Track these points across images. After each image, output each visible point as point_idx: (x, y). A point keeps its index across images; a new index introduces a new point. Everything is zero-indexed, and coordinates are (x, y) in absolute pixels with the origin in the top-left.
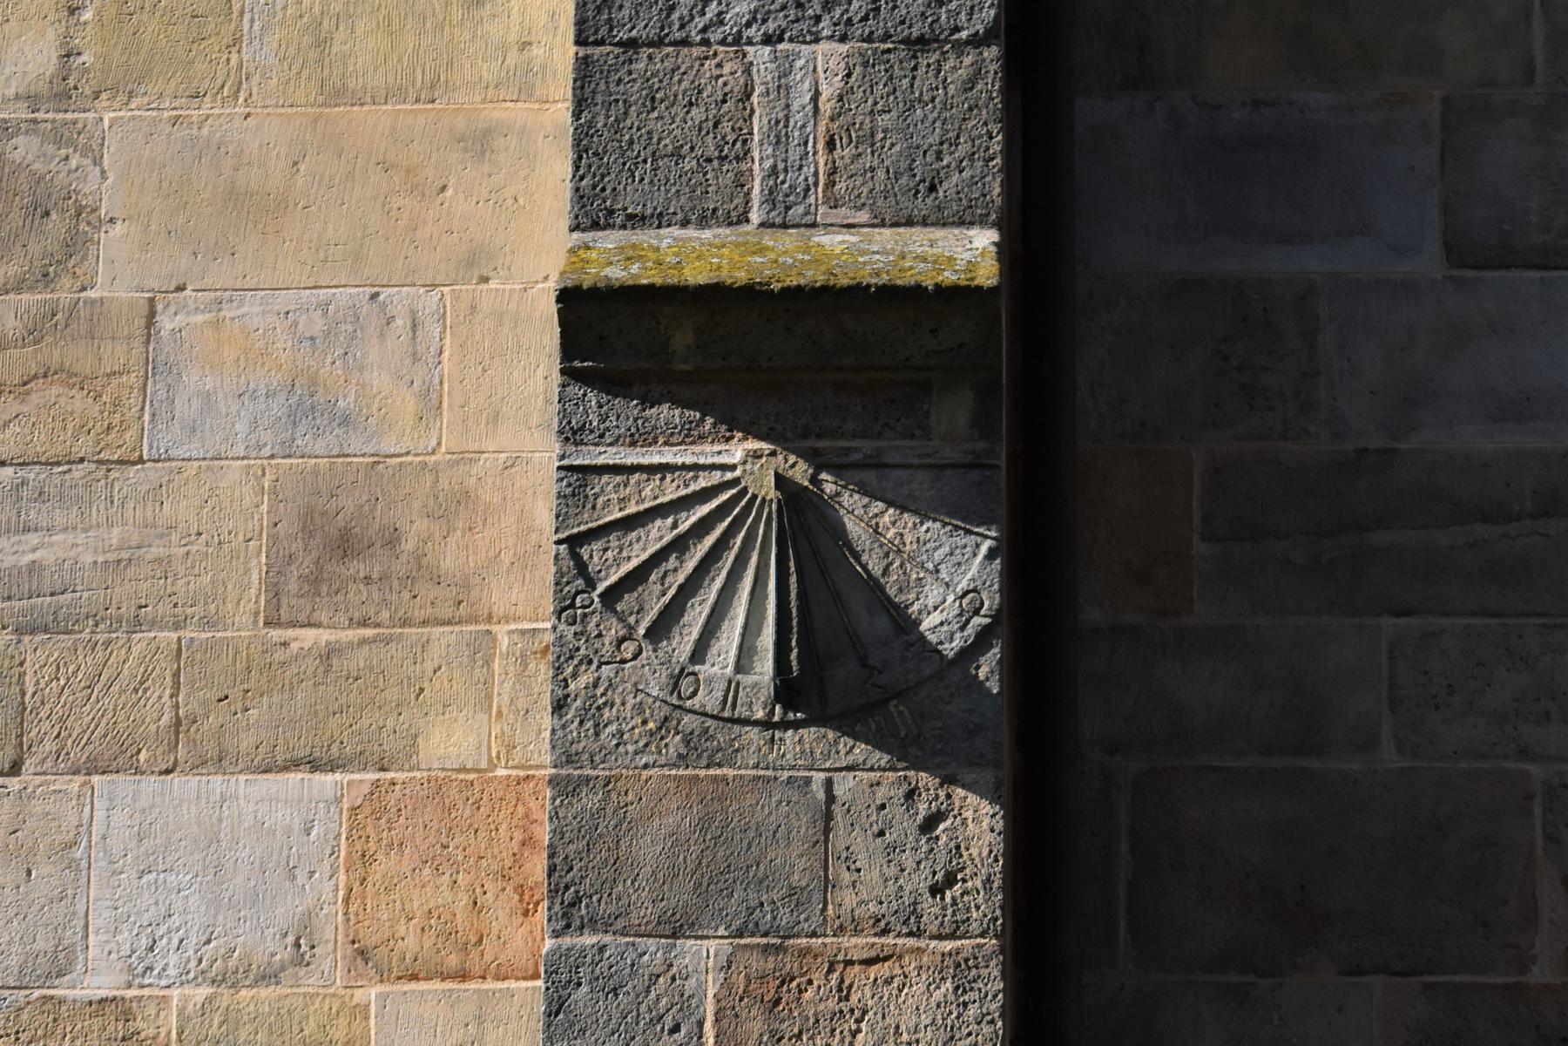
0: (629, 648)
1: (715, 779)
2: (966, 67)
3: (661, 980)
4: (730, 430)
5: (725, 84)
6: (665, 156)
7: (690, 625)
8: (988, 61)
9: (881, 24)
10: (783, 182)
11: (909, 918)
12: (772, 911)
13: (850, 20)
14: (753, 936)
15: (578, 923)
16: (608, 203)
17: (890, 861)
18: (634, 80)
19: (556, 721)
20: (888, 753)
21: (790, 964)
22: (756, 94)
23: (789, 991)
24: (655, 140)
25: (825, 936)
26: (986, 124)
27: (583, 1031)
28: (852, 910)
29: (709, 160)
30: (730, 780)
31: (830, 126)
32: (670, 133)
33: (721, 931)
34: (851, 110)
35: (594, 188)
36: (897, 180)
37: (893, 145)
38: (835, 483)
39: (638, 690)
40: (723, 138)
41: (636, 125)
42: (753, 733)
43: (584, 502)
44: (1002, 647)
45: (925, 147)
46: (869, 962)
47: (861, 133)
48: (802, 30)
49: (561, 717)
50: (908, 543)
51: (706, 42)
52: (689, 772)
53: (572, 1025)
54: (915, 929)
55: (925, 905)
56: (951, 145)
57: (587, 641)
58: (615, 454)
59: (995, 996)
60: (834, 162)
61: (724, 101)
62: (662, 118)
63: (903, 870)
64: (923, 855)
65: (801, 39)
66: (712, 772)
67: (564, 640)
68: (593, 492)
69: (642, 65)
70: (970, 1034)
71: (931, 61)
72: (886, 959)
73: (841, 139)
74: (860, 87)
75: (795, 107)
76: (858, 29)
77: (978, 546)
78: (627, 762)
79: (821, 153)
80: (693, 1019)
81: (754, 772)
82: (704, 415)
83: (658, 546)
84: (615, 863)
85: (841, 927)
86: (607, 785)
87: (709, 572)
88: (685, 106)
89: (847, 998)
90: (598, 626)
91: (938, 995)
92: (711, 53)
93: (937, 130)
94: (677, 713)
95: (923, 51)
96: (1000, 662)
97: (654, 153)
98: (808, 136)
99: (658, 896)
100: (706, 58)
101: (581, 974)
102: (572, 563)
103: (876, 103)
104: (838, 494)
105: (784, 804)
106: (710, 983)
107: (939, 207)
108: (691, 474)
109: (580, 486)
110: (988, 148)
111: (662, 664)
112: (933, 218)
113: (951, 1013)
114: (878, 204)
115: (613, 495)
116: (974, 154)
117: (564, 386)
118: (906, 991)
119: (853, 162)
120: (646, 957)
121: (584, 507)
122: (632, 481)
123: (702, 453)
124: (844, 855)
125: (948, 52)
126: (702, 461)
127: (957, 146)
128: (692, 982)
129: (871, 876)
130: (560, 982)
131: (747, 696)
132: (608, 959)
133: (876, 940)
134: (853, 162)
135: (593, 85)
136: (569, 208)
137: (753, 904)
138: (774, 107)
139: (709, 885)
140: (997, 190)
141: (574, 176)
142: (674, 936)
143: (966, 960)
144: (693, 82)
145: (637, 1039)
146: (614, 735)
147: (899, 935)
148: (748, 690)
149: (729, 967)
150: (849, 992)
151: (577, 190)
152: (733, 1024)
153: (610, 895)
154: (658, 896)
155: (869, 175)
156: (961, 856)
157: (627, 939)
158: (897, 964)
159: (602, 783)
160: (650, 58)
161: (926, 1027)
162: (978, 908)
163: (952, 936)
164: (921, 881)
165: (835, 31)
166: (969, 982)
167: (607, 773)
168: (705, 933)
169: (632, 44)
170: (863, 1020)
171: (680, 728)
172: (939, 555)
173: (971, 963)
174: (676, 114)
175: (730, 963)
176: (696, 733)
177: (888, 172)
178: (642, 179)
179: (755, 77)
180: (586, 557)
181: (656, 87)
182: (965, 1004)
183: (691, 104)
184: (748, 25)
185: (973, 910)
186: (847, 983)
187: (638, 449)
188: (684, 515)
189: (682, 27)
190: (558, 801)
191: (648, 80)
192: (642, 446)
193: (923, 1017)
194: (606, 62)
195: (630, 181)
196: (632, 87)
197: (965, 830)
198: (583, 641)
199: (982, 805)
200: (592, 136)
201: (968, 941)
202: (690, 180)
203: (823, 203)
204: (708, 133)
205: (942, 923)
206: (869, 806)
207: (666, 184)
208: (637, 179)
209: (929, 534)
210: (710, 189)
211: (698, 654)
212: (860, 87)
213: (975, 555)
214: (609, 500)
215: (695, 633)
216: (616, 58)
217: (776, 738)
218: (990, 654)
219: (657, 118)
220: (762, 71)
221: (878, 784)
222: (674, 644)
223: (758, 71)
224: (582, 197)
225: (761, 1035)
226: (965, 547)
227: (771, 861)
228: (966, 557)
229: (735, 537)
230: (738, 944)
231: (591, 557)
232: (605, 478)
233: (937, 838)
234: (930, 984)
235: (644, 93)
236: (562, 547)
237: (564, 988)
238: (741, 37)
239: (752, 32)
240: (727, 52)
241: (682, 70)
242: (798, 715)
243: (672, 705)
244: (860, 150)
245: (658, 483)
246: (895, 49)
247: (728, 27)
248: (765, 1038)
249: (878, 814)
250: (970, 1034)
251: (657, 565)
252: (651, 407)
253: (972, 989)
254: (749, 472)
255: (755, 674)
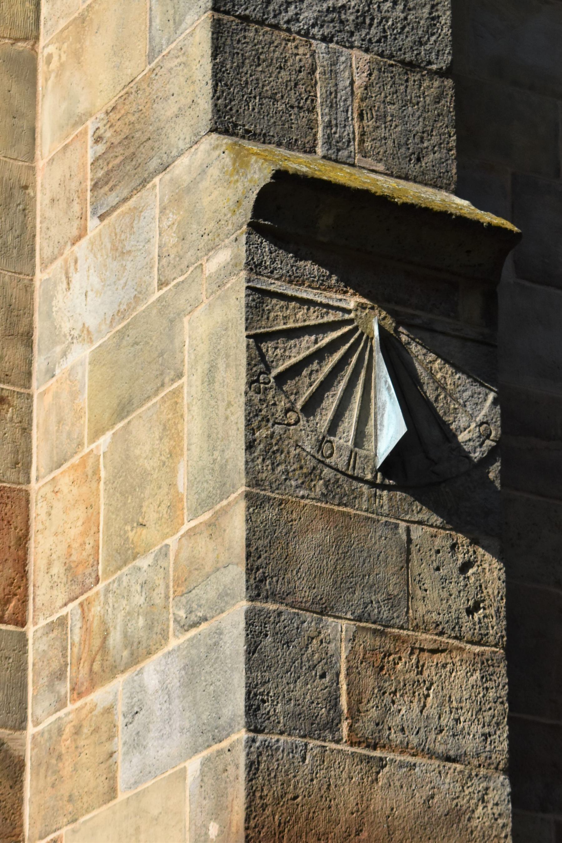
0: (292, 417)
1: (343, 514)
2: (436, 88)
3: (314, 641)
4: (346, 287)
5: (300, 60)
6: (267, 97)
7: (326, 409)
8: (447, 88)
9: (388, 47)
10: (335, 133)
11: (455, 627)
12: (378, 608)
13: (370, 39)
14: (367, 622)
15: (265, 594)
16: (234, 119)
17: (443, 588)
18: (247, 43)
19: (248, 456)
20: (441, 517)
21: (389, 645)
22: (318, 71)
23: (388, 662)
24: (260, 85)
25: (408, 630)
26: (447, 127)
27: (269, 667)
28: (423, 616)
29: (292, 107)
30: (352, 516)
31: (361, 104)
32: (269, 83)
33: (349, 616)
34: (372, 97)
35: (226, 107)
36: (399, 149)
37: (396, 126)
38: (408, 336)
39: (297, 445)
40: (300, 95)
41: (249, 72)
42: (365, 488)
43: (262, 314)
44: (501, 463)
45: (414, 132)
46: (434, 652)
47: (378, 113)
48: (343, 38)
49: (251, 454)
50: (449, 384)
51: (288, 30)
52: (327, 506)
53: (263, 662)
54: (458, 635)
55: (464, 620)
56: (428, 135)
57: (267, 406)
58: (280, 286)
59: (504, 686)
60: (364, 128)
61: (300, 71)
62: (264, 72)
63: (451, 595)
64: (462, 588)
65: (343, 44)
66: (341, 509)
67: (252, 402)
68: (267, 308)
69: (252, 34)
70: (490, 709)
71: (416, 79)
72: (443, 651)
73: (367, 114)
74: (377, 84)
75: (341, 86)
76: (375, 46)
77: (487, 395)
78: (292, 492)
79: (356, 120)
80: (334, 671)
81: (365, 514)
82: (331, 273)
83: (307, 353)
84: (286, 558)
85: (417, 626)
86: (280, 505)
87: (337, 377)
88: (277, 68)
89: (421, 673)
90: (274, 397)
91: (472, 680)
92: (292, 38)
93: (421, 124)
94: (320, 466)
95: (411, 71)
96: (500, 471)
97: (260, 94)
98: (348, 107)
99: (312, 585)
100: (289, 40)
101: (268, 629)
102: (257, 353)
103: (386, 97)
104: (409, 343)
105: (383, 538)
106: (343, 648)
107: (423, 172)
108: (325, 310)
109: (260, 303)
110: (448, 143)
111: (312, 431)
112: (419, 179)
113: (479, 693)
114: (389, 161)
115: (279, 313)
116: (441, 144)
117: (249, 234)
118: (454, 674)
119: (374, 131)
120: (305, 624)
121: (262, 317)
122: (291, 307)
123: (330, 298)
124: (418, 578)
125: (425, 75)
126: (331, 303)
127: (431, 136)
128: (332, 646)
129: (433, 595)
130: (255, 631)
131: (362, 463)
132: (283, 621)
133: (436, 637)
134: (374, 131)
135: (223, 39)
136: (210, 116)
137: (368, 600)
138: (329, 84)
139: (341, 583)
140: (454, 171)
141: (214, 96)
142: (321, 613)
143: (487, 660)
144: (282, 54)
145: (301, 678)
146: (283, 473)
147: (449, 637)
148: (362, 459)
149: (354, 640)
150: (422, 669)
151: (216, 105)
152: (358, 678)
153: (283, 578)
154: (312, 585)
155: (383, 141)
156: (482, 592)
157: (294, 610)
158: (449, 656)
159: (278, 503)
160: (256, 30)
161: (466, 699)
162: (493, 627)
163: (478, 643)
164: (461, 604)
165: (362, 44)
166: (489, 674)
167: (280, 497)
168: (340, 615)
169: (245, 19)
170: (430, 689)
171: (322, 475)
172: (466, 395)
173: (490, 662)
174: (272, 72)
175: (354, 637)
176: (332, 482)
177: (394, 142)
178: (253, 109)
179: (317, 61)
180: (264, 350)
181: (260, 51)
182: (487, 689)
183: (281, 68)
184: (313, 26)
185: (490, 628)
186: (421, 663)
187: (293, 286)
188: (321, 336)
189: (275, 16)
190: (251, 510)
191: (255, 45)
192: (296, 285)
193: (464, 693)
194: (231, 26)
195: (246, 108)
196: (246, 47)
197: (484, 576)
198: (264, 406)
199: (493, 562)
200: (224, 72)
201: (487, 648)
202: (282, 117)
203: (359, 153)
204: (291, 89)
205: (474, 634)
206: (431, 550)
207: (267, 116)
208: (251, 108)
209: (460, 381)
210: (293, 126)
211: (333, 428)
212: (377, 84)
213: (485, 400)
214: (277, 316)
215: (330, 415)
216: (237, 25)
217: (378, 494)
218: (495, 466)
219: (261, 71)
220: (321, 58)
221: (435, 536)
222: (318, 419)
223: (319, 57)
224: (219, 111)
225: (373, 688)
226: (479, 393)
227: (377, 575)
228: (480, 400)
229: (351, 357)
230: (359, 626)
231: (267, 351)
232: (274, 301)
233: (468, 578)
234: (467, 673)
235: (254, 53)
236: (251, 340)
237: (258, 636)
238: (309, 33)
239: (315, 30)
240: (301, 40)
241: (275, 44)
242: (391, 481)
243: (318, 460)
244: (378, 124)
245: (305, 311)
246: (396, 65)
247: (301, 24)
248: (376, 691)
249: (436, 556)
250: (490, 709)
251: (307, 366)
252: (301, 260)
253: (491, 680)
254: (359, 316)
255: (364, 449)
